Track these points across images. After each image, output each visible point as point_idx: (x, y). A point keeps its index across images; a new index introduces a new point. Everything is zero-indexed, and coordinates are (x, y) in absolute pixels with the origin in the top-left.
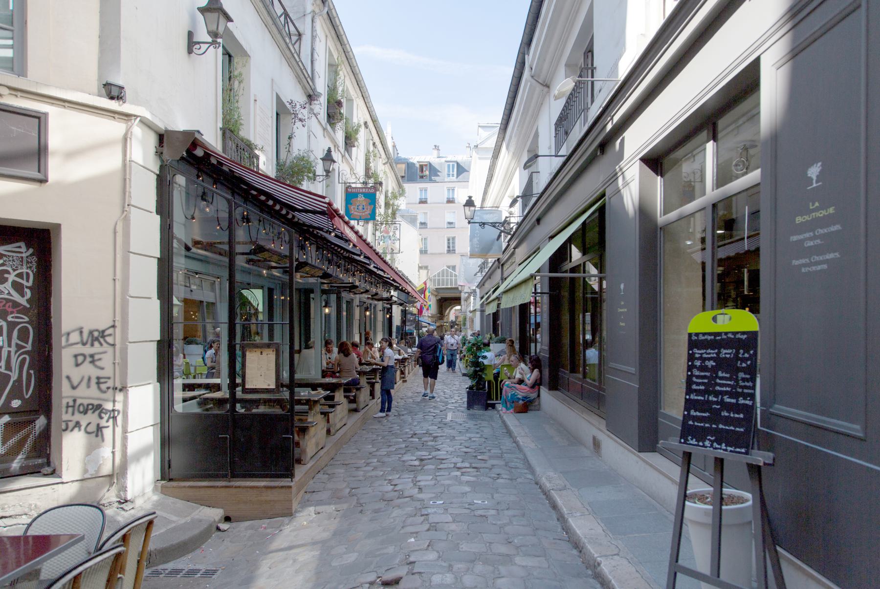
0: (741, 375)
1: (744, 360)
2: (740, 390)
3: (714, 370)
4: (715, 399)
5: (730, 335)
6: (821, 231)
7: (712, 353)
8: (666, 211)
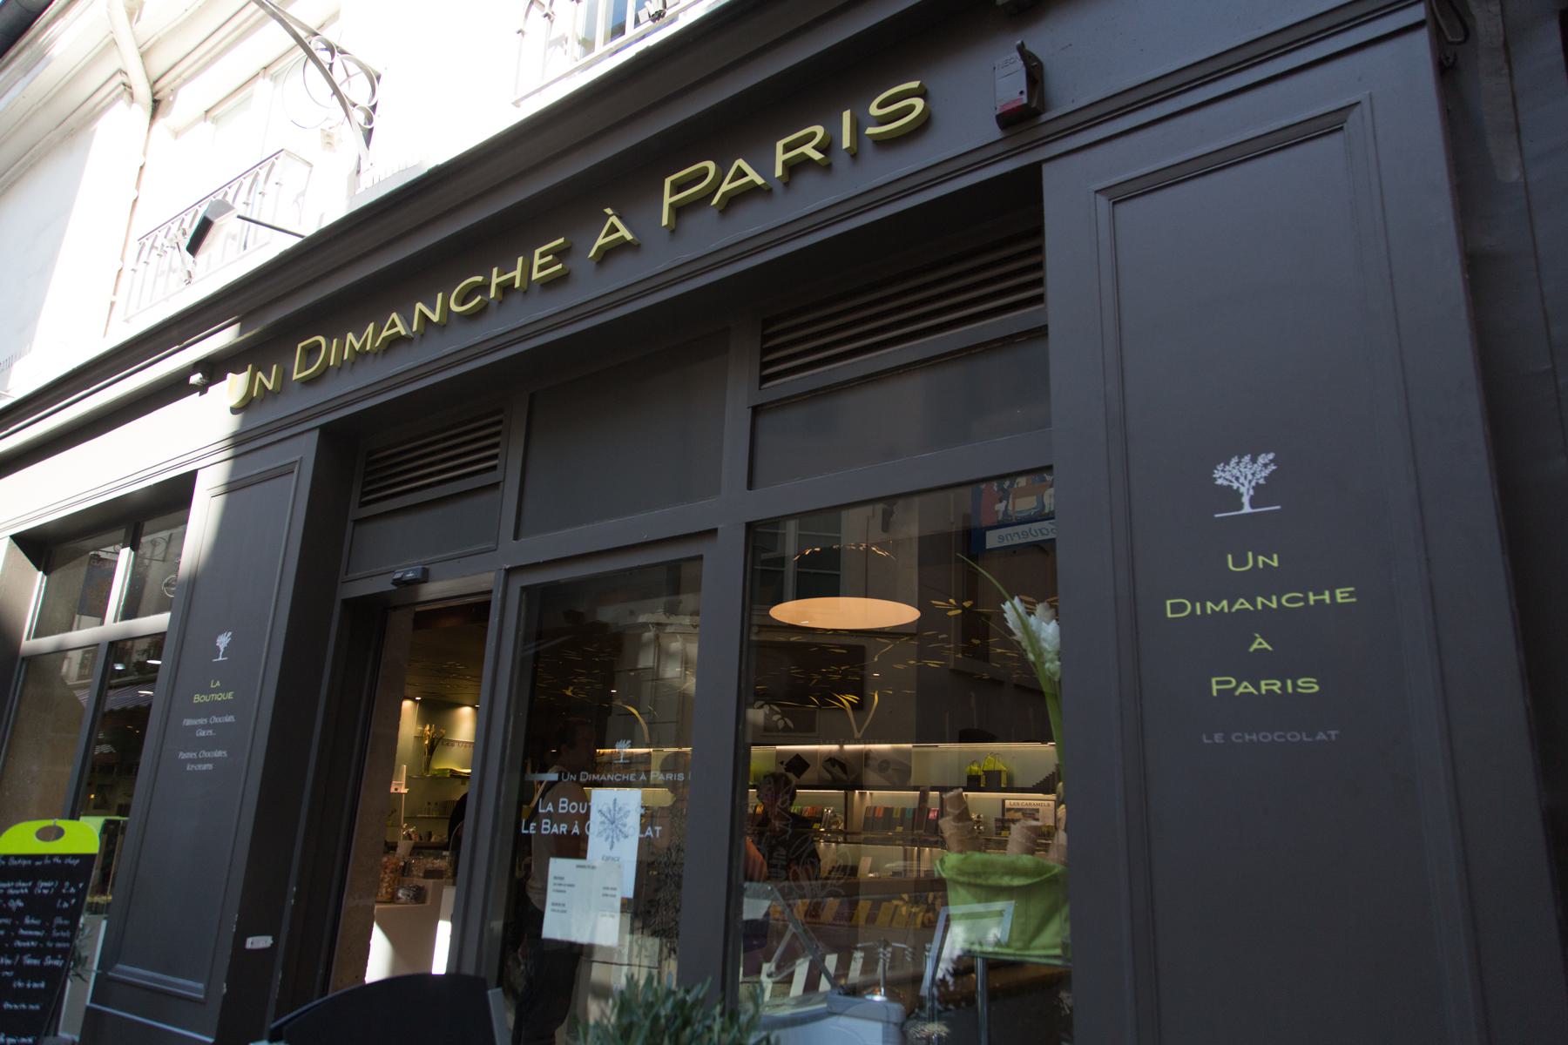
0: (59, 921)
1: (67, 897)
2: (50, 944)
3: (20, 914)
4: (8, 962)
5: (57, 860)
6: (216, 720)
7: (23, 887)
8: (39, 632)
